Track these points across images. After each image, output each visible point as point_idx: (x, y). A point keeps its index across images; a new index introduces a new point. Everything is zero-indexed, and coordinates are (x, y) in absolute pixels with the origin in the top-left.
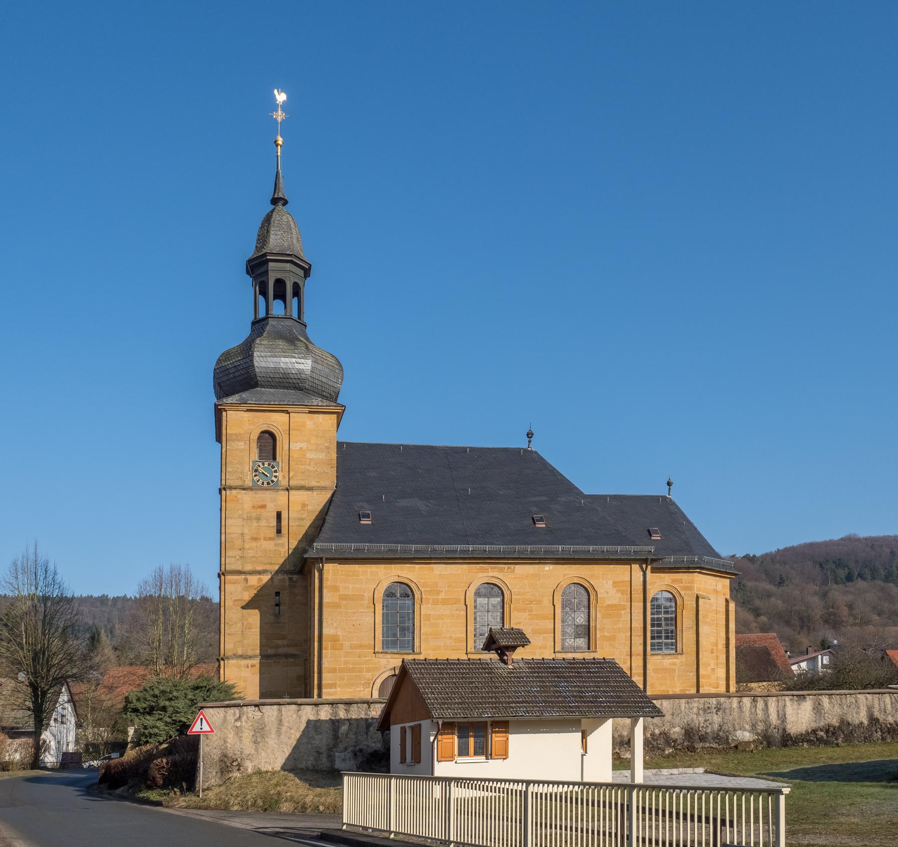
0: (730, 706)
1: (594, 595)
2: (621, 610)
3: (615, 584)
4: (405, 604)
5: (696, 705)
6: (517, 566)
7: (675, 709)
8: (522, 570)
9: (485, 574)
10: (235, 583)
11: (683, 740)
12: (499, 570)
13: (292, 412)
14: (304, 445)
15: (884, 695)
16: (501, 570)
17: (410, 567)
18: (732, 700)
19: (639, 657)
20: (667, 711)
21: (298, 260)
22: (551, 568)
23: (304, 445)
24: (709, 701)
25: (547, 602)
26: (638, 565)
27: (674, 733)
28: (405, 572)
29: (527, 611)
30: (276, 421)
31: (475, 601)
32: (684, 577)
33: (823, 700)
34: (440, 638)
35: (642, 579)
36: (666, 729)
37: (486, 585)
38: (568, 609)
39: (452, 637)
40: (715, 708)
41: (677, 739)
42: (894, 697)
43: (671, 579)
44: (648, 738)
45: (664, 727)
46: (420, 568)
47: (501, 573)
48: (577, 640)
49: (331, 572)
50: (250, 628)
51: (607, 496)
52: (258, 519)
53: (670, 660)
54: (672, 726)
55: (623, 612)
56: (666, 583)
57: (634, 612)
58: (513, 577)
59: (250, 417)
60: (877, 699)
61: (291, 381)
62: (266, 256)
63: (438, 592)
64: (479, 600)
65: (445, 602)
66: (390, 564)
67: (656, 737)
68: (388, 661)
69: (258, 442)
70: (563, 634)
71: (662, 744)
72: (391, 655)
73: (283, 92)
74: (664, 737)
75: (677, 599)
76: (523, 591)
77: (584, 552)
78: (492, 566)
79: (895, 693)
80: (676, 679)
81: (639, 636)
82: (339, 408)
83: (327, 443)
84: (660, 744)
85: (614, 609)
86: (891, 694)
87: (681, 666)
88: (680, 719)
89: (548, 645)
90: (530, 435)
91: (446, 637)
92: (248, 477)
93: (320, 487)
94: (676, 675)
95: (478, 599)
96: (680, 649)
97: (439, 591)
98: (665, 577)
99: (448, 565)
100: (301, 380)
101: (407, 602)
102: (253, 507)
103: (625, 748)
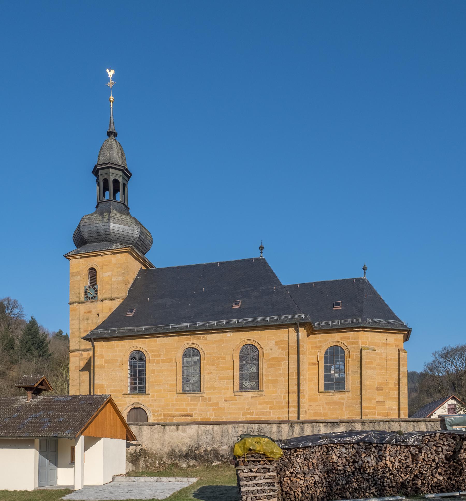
0: (270, 430)
1: (262, 351)
2: (281, 361)
3: (277, 343)
4: (141, 363)
5: (241, 429)
6: (209, 335)
7: (224, 432)
8: (212, 337)
9: (188, 342)
10: (75, 357)
11: (229, 455)
12: (197, 338)
13: (104, 255)
14: (110, 273)
15: (419, 423)
16: (199, 339)
17: (143, 341)
18: (272, 425)
19: (295, 394)
20: (218, 433)
21: (113, 165)
22: (232, 335)
23: (110, 273)
24: (252, 426)
25: (228, 358)
26: (293, 329)
27: (222, 450)
28: (140, 344)
29: (215, 365)
30: (96, 262)
31: (183, 360)
32: (351, 335)
33: (355, 426)
34: (161, 384)
35: (296, 338)
36: (216, 447)
37: (190, 349)
38: (244, 362)
39: (168, 384)
40: (257, 432)
41: (224, 455)
42: (430, 424)
43: (340, 337)
44: (201, 453)
45: (214, 445)
46: (149, 341)
47: (198, 341)
48: (251, 383)
49: (99, 346)
50: (84, 382)
51: (313, 283)
52: (87, 319)
53: (340, 396)
54: (221, 445)
55: (283, 362)
56: (336, 340)
57: (291, 362)
58: (206, 342)
59: (83, 261)
60: (411, 426)
61: (102, 237)
62: (97, 167)
63: (160, 355)
64: (186, 359)
65: (164, 361)
66: (132, 339)
67: (207, 453)
68: (131, 399)
69: (89, 275)
70: (241, 379)
71: (211, 458)
72: (132, 396)
73: (112, 69)
74: (213, 453)
75: (345, 351)
76: (213, 351)
77: (253, 322)
78: (193, 336)
79: (431, 421)
80: (344, 409)
81: (294, 379)
82: (127, 248)
83: (123, 270)
84: (210, 458)
85: (275, 362)
86: (426, 422)
87: (348, 400)
88: (228, 440)
89: (230, 387)
90: (262, 248)
91: (164, 384)
92: (82, 296)
93: (119, 297)
94: (344, 407)
95: (185, 359)
96: (347, 388)
97: (160, 354)
98: (335, 336)
99: (166, 338)
100: (107, 235)
101: (142, 362)
102: (85, 313)
103: (183, 459)
